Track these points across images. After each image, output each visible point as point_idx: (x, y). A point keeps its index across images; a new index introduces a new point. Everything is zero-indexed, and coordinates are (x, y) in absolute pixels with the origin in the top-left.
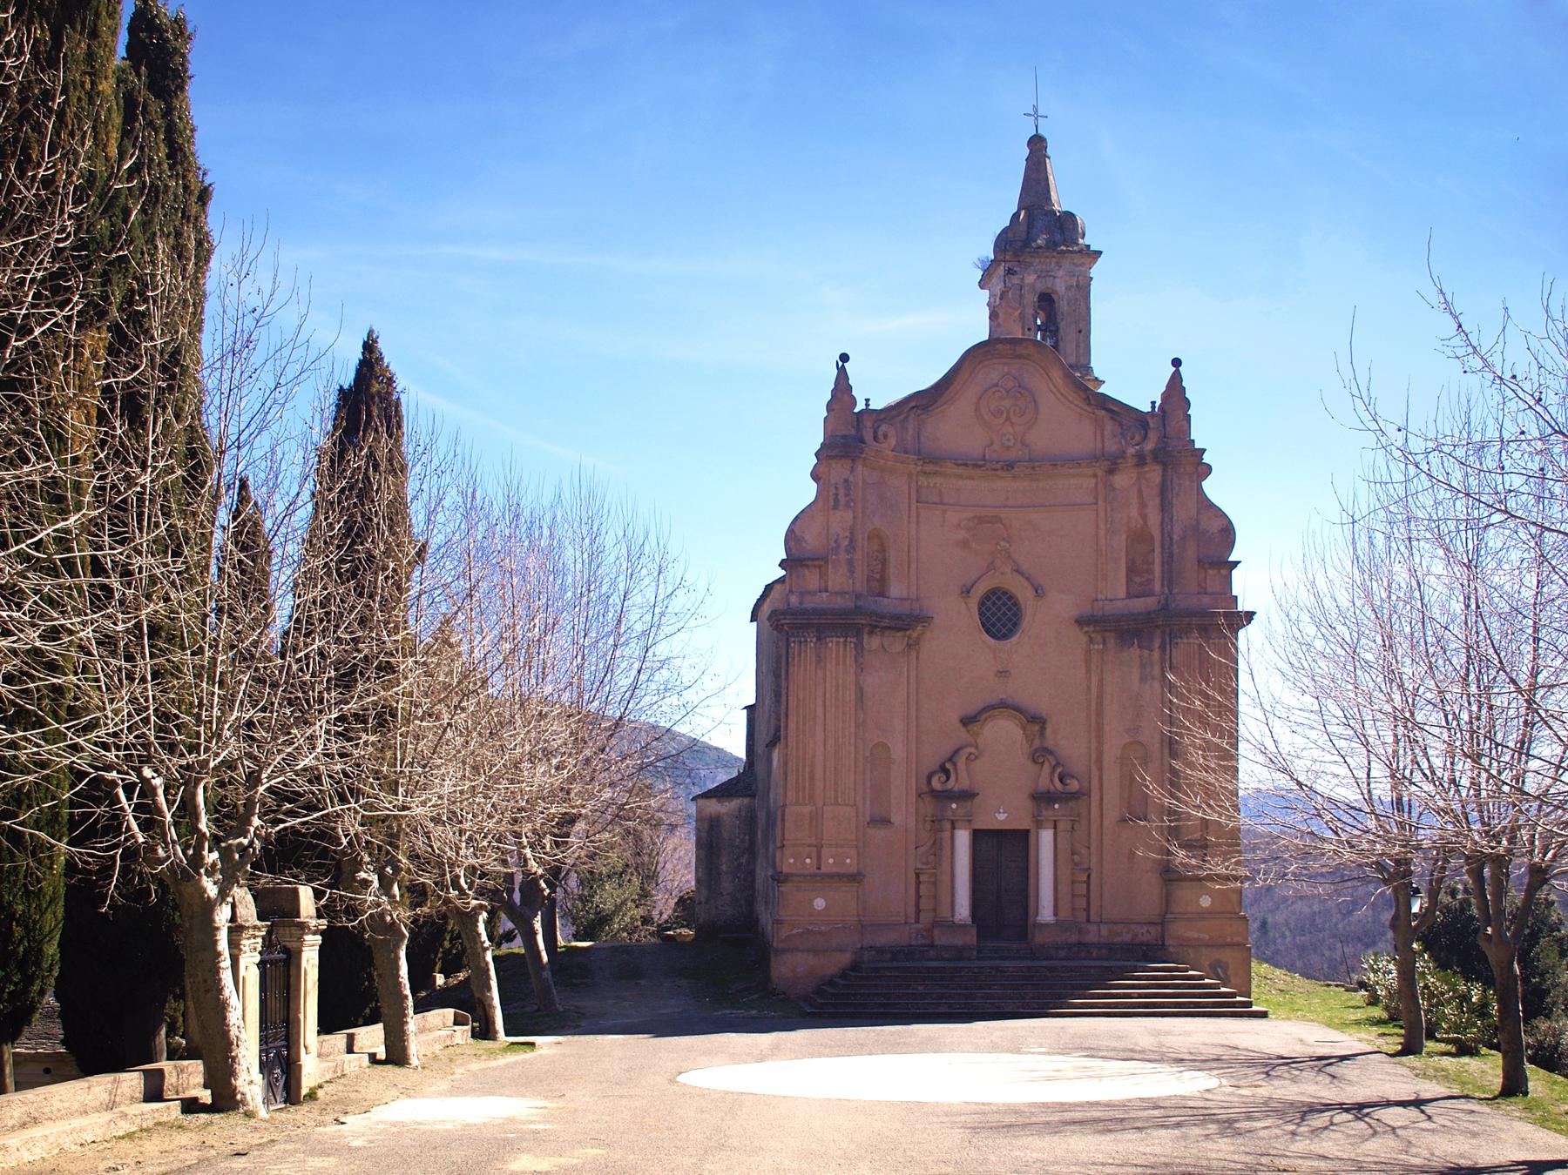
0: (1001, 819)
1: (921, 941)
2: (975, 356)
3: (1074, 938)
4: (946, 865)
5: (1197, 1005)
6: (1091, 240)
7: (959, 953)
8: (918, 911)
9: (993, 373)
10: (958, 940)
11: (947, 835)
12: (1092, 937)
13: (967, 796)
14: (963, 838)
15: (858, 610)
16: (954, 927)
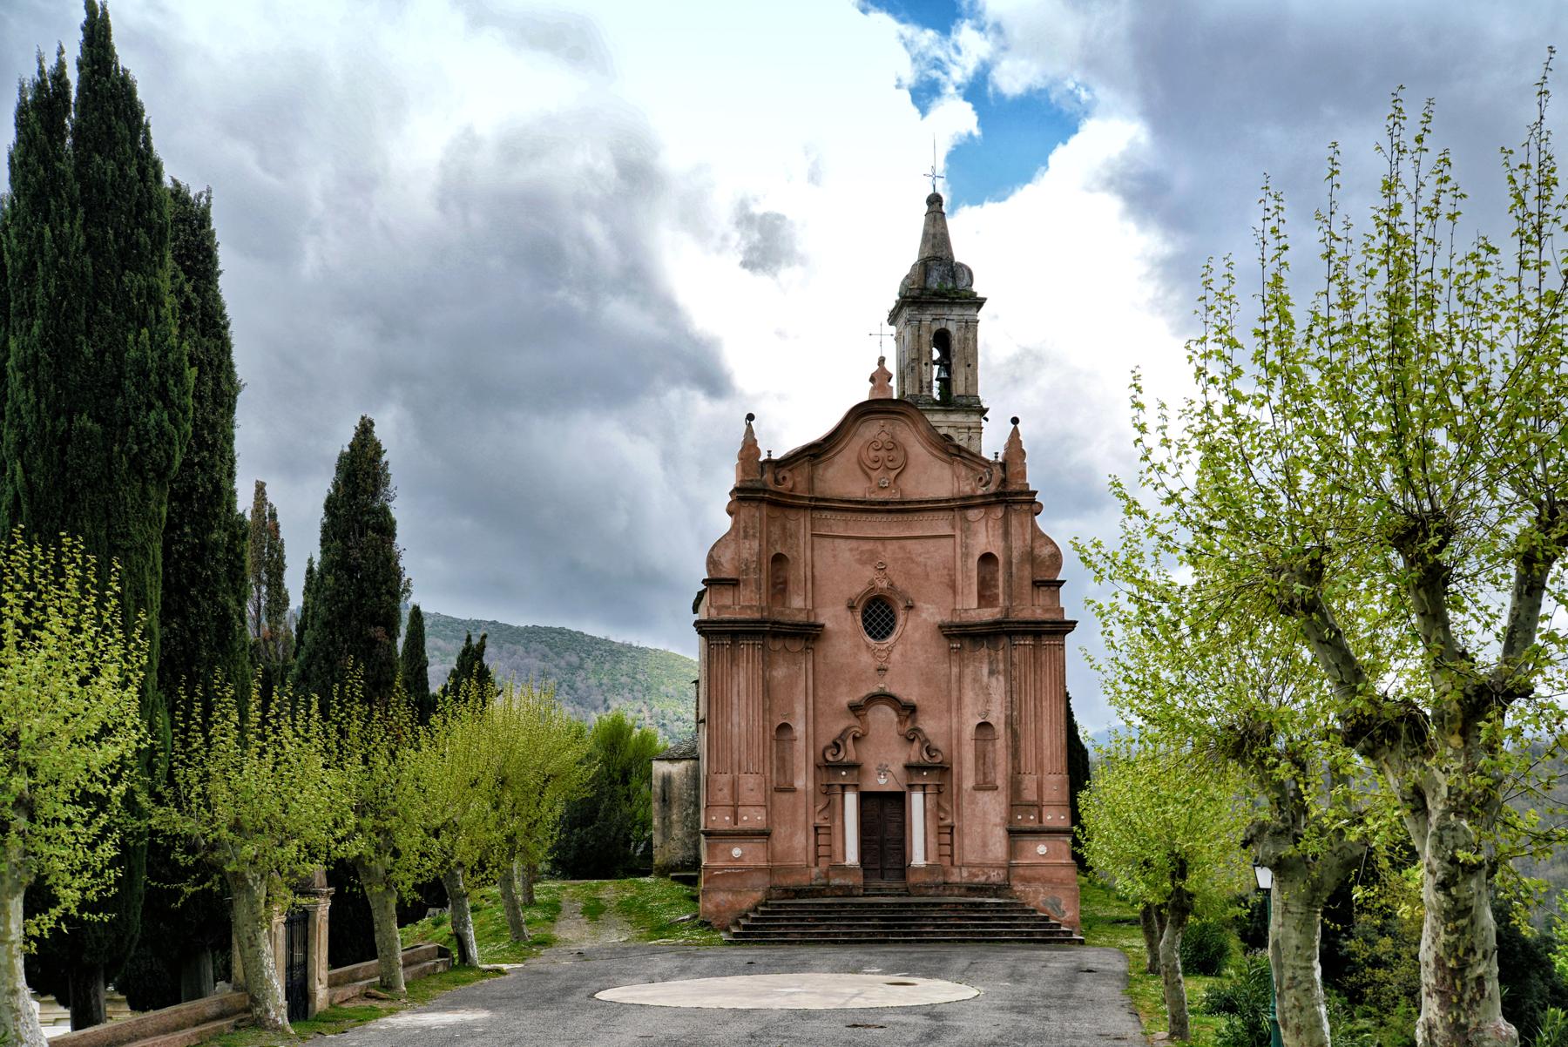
0: (882, 783)
1: (820, 881)
2: (860, 413)
3: (940, 879)
4: (838, 822)
5: (983, 934)
6: (979, 288)
7: (847, 891)
8: (817, 857)
9: (872, 430)
10: (849, 881)
11: (838, 797)
12: (955, 878)
13: (854, 767)
14: (851, 799)
15: (761, 622)
16: (845, 870)
